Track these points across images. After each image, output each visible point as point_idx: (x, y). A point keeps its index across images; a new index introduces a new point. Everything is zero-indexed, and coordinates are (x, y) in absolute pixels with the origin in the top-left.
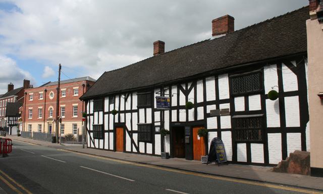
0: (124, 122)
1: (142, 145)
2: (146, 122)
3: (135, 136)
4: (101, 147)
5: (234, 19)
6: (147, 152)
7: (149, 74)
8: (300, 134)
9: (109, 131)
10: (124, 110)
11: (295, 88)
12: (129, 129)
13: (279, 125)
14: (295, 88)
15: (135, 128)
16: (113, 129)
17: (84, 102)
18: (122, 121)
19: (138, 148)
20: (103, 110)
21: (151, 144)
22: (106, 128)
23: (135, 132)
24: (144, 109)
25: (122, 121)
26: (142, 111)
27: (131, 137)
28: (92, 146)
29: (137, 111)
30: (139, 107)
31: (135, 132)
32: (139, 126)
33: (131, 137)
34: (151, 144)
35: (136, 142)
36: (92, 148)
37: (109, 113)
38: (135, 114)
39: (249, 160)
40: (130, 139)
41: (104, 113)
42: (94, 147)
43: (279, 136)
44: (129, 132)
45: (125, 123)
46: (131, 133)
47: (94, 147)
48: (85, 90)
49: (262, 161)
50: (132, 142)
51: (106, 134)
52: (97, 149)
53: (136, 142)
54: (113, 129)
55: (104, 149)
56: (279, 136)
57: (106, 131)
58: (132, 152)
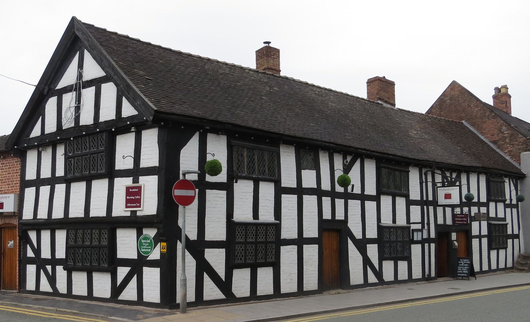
0: (343, 218)
1: (388, 267)
3: (373, 251)
4: (403, 274)
5: (394, 85)
6: (96, 294)
7: (152, 113)
8: (225, 192)
12: (358, 235)
13: (294, 185)
15: (372, 233)
17: (425, 199)
18: (340, 215)
19: (379, 274)
22: (485, 241)
23: (372, 241)
25: (340, 215)
26: (492, 205)
28: (45, 286)
29: (376, 199)
30: (489, 200)
31: (372, 241)
32: (381, 229)
33: (363, 251)
39: (90, 295)
40: (360, 258)
42: (50, 290)
44: (356, 242)
45: (345, 221)
47: (50, 290)
49: (85, 294)
50: (367, 262)
52: (62, 295)
55: (490, 271)
58: (37, 290)
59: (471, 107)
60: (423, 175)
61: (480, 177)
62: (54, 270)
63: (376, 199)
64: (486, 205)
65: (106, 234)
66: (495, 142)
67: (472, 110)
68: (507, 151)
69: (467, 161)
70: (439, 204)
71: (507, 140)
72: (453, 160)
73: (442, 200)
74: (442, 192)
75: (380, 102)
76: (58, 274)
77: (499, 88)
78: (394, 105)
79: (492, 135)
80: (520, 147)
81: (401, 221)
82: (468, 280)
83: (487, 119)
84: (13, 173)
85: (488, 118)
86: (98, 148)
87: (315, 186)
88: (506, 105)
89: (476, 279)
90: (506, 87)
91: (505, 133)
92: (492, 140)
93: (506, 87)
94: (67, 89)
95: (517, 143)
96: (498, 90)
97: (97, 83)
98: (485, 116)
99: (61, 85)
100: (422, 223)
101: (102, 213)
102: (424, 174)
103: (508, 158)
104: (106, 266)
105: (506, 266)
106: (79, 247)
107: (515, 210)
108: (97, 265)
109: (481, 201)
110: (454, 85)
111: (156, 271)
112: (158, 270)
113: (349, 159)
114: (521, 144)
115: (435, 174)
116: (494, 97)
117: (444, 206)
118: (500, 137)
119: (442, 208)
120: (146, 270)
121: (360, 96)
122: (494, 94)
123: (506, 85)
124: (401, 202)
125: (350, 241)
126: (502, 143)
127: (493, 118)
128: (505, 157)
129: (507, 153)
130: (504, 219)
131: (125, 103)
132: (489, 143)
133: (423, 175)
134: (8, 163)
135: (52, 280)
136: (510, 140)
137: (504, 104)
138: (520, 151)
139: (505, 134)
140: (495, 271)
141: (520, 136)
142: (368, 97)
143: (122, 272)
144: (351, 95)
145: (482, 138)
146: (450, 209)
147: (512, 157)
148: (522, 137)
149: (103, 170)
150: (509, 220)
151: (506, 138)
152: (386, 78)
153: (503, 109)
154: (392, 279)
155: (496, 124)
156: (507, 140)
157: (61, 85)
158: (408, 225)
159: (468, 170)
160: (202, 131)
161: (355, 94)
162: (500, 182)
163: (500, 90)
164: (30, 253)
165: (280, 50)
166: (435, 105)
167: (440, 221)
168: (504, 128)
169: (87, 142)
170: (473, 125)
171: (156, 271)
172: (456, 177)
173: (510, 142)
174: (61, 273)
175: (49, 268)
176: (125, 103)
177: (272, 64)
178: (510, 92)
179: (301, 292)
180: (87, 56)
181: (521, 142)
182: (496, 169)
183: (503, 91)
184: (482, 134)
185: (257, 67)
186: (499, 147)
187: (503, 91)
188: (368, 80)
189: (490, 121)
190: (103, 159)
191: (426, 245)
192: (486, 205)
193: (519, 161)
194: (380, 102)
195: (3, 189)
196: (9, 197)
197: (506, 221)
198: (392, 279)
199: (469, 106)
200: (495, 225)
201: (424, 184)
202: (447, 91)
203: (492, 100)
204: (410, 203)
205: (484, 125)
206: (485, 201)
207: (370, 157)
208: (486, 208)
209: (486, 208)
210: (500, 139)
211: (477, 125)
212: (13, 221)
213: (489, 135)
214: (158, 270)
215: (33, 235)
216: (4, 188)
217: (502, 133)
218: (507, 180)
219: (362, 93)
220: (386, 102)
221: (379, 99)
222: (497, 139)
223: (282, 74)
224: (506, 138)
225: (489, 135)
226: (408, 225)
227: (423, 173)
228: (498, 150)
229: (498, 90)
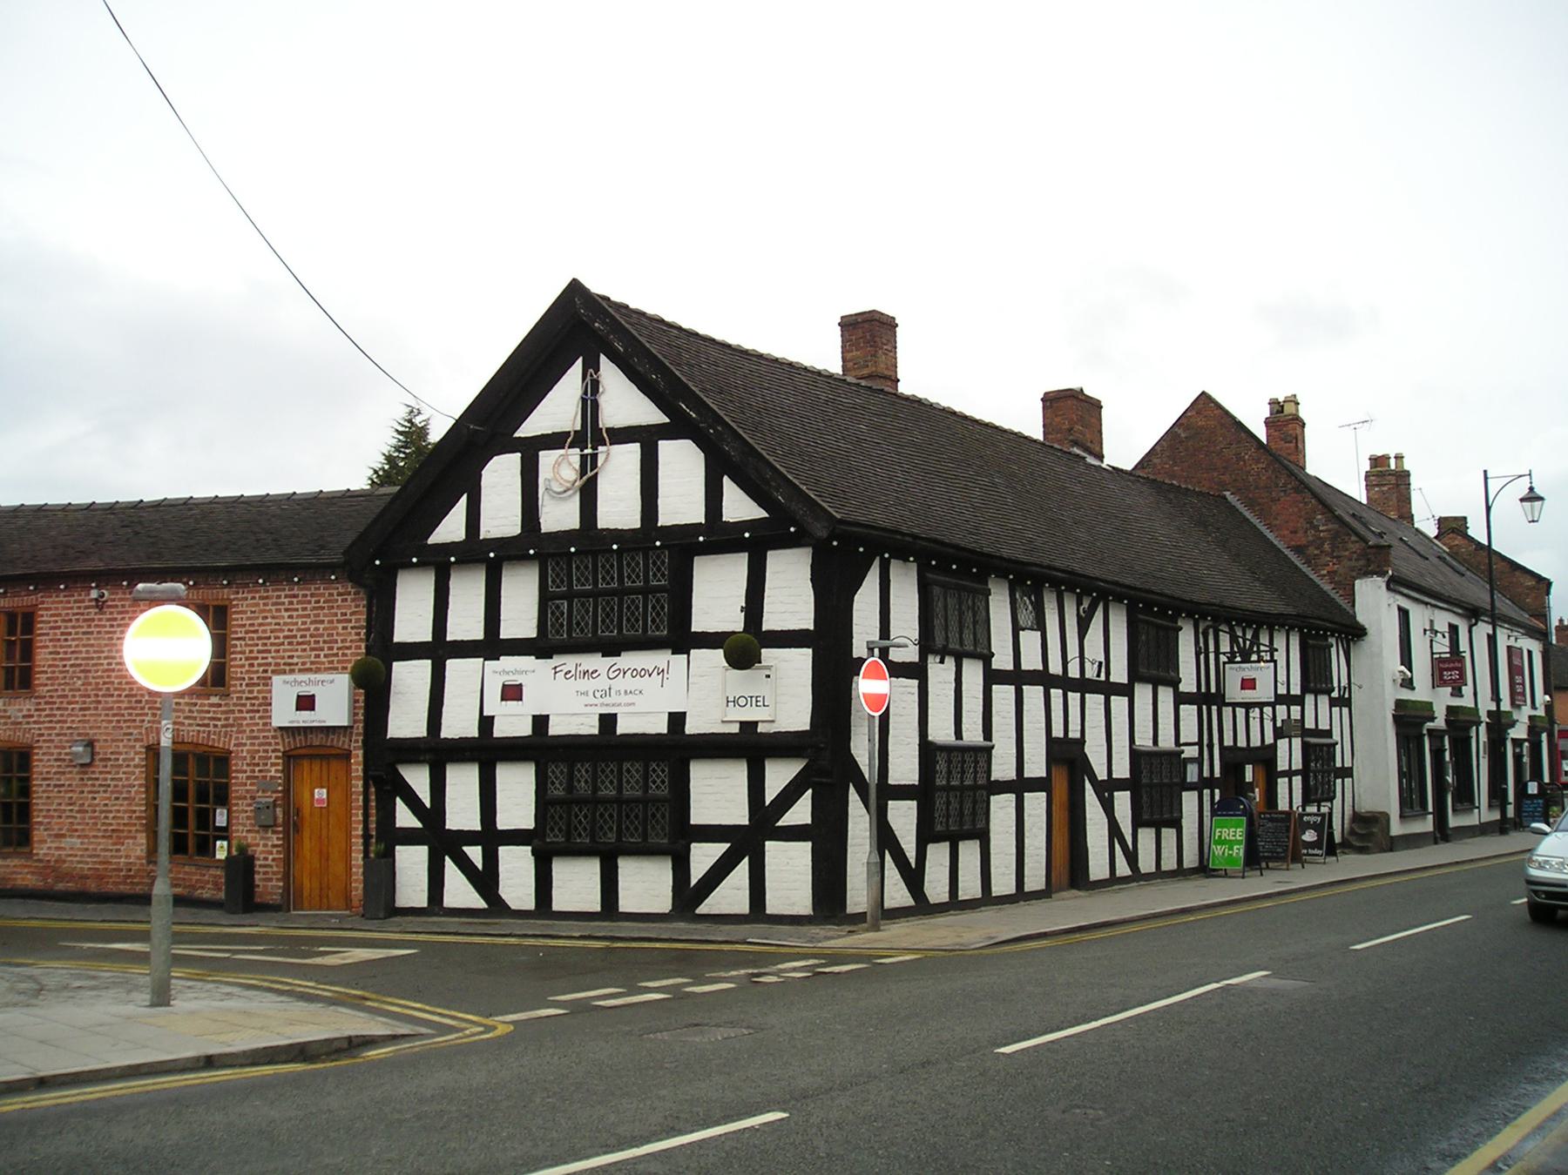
2: (1155, 742)
3: (903, 817)
4: (970, 887)
9: (1020, 786)
10: (1319, 697)
11: (804, 619)
12: (1102, 775)
14: (804, 619)
15: (1122, 770)
16: (1127, 775)
20: (1174, 683)
21: (1174, 831)
22: (1002, 768)
24: (1025, 666)
26: (1143, 693)
27: (1108, 807)
29: (1127, 690)
33: (1108, 807)
34: (1174, 831)
35: (909, 847)
36: (1125, 880)
37: (1018, 678)
38: (1119, 704)
41: (992, 677)
43: (504, 822)
45: (1081, 742)
46: (1106, 790)
48: (1486, 619)
51: (1001, 808)
53: (909, 847)
54: (1127, 775)
55: (987, 898)
56: (504, 822)
57: (1296, 773)
59: (1244, 461)
60: (1201, 636)
61: (1291, 638)
62: (491, 859)
63: (1127, 690)
64: (1299, 701)
65: (663, 771)
66: (1298, 550)
67: (1248, 468)
68: (1325, 572)
69: (1278, 607)
70: (1227, 701)
71: (1327, 547)
72: (1245, 602)
73: (1234, 692)
74: (1234, 675)
75: (1076, 450)
76: (852, 839)
77: (1281, 399)
78: (1101, 457)
79: (1291, 532)
80: (1353, 563)
81: (1167, 742)
82: (1288, 869)
83: (1282, 494)
84: (331, 622)
85: (1285, 491)
86: (649, 582)
87: (1041, 668)
88: (1297, 447)
89: (1262, 875)
90: (1293, 401)
91: (1321, 528)
92: (1293, 543)
93: (1293, 401)
94: (555, 441)
95: (1347, 553)
96: (1378, 461)
97: (647, 438)
98: (1277, 486)
99: (531, 427)
100: (1200, 743)
101: (1258, 744)
102: (1203, 634)
103: (1327, 587)
104: (665, 841)
105: (1115, 874)
106: (581, 802)
107: (1345, 710)
108: (640, 840)
109: (1025, 666)
110: (1204, 402)
111: (802, 852)
112: (807, 846)
113: (1086, 604)
114: (1355, 556)
115: (1221, 633)
116: (1267, 423)
117: (1234, 705)
118: (1311, 538)
119: (1231, 708)
120: (774, 850)
121: (807, 359)
122: (1268, 415)
123: (1295, 396)
124: (1166, 695)
125: (1088, 785)
126: (1316, 552)
127: (1295, 492)
128: (1322, 586)
129: (1325, 575)
130: (1329, 733)
131: (730, 488)
132: (1287, 552)
133: (1201, 636)
134: (312, 595)
135: (486, 880)
136: (1333, 547)
137: (1291, 442)
138: (1354, 574)
139: (1322, 531)
140: (971, 905)
141: (1354, 538)
142: (1045, 434)
143: (704, 856)
144: (797, 363)
145: (1271, 536)
146: (1244, 710)
147: (1337, 585)
148: (1357, 542)
149: (612, 632)
150: (1336, 736)
151: (1323, 540)
152: (1086, 392)
153: (1289, 454)
154: (945, 897)
155: (1301, 505)
156: (1327, 547)
157: (531, 427)
158: (1178, 749)
159: (1272, 622)
160: (1011, 577)
161: (819, 366)
162: (974, 592)
163: (1282, 406)
164: (405, 818)
165: (1553, 584)
166: (1158, 448)
167: (1228, 742)
168: (1319, 517)
169: (612, 566)
170: (1250, 505)
171: (802, 852)
172: (1253, 636)
173: (1333, 551)
174: (516, 867)
175: (475, 853)
176: (730, 488)
177: (882, 366)
178: (1302, 414)
179: (1021, 895)
180: (610, 374)
181: (1355, 552)
182: (1319, 618)
183: (1289, 409)
184: (1270, 526)
185: (844, 367)
186: (1308, 563)
187: (1289, 409)
188: (1046, 394)
189: (1288, 499)
190: (662, 608)
191: (1206, 792)
192: (1299, 701)
193: (1351, 596)
194: (1076, 450)
195: (295, 660)
196: (332, 682)
197: (1331, 737)
198: (945, 897)
199: (1239, 458)
200: (1316, 745)
201: (1202, 657)
202: (1189, 414)
203: (1264, 429)
204: (1180, 699)
205: (1274, 507)
206: (1299, 693)
207: (1119, 599)
208: (916, 682)
209: (916, 682)
210: (1311, 543)
211: (1259, 504)
212: (338, 741)
213: (1286, 532)
214: (807, 846)
215: (418, 779)
216: (298, 657)
217: (1316, 528)
218: (1332, 641)
219: (1031, 424)
220: (1091, 453)
221: (1076, 443)
222: (1304, 541)
223: (904, 388)
224: (1323, 540)
225: (1286, 532)
226: (1178, 749)
227: (1201, 630)
228: (1305, 568)
229: (1378, 461)
